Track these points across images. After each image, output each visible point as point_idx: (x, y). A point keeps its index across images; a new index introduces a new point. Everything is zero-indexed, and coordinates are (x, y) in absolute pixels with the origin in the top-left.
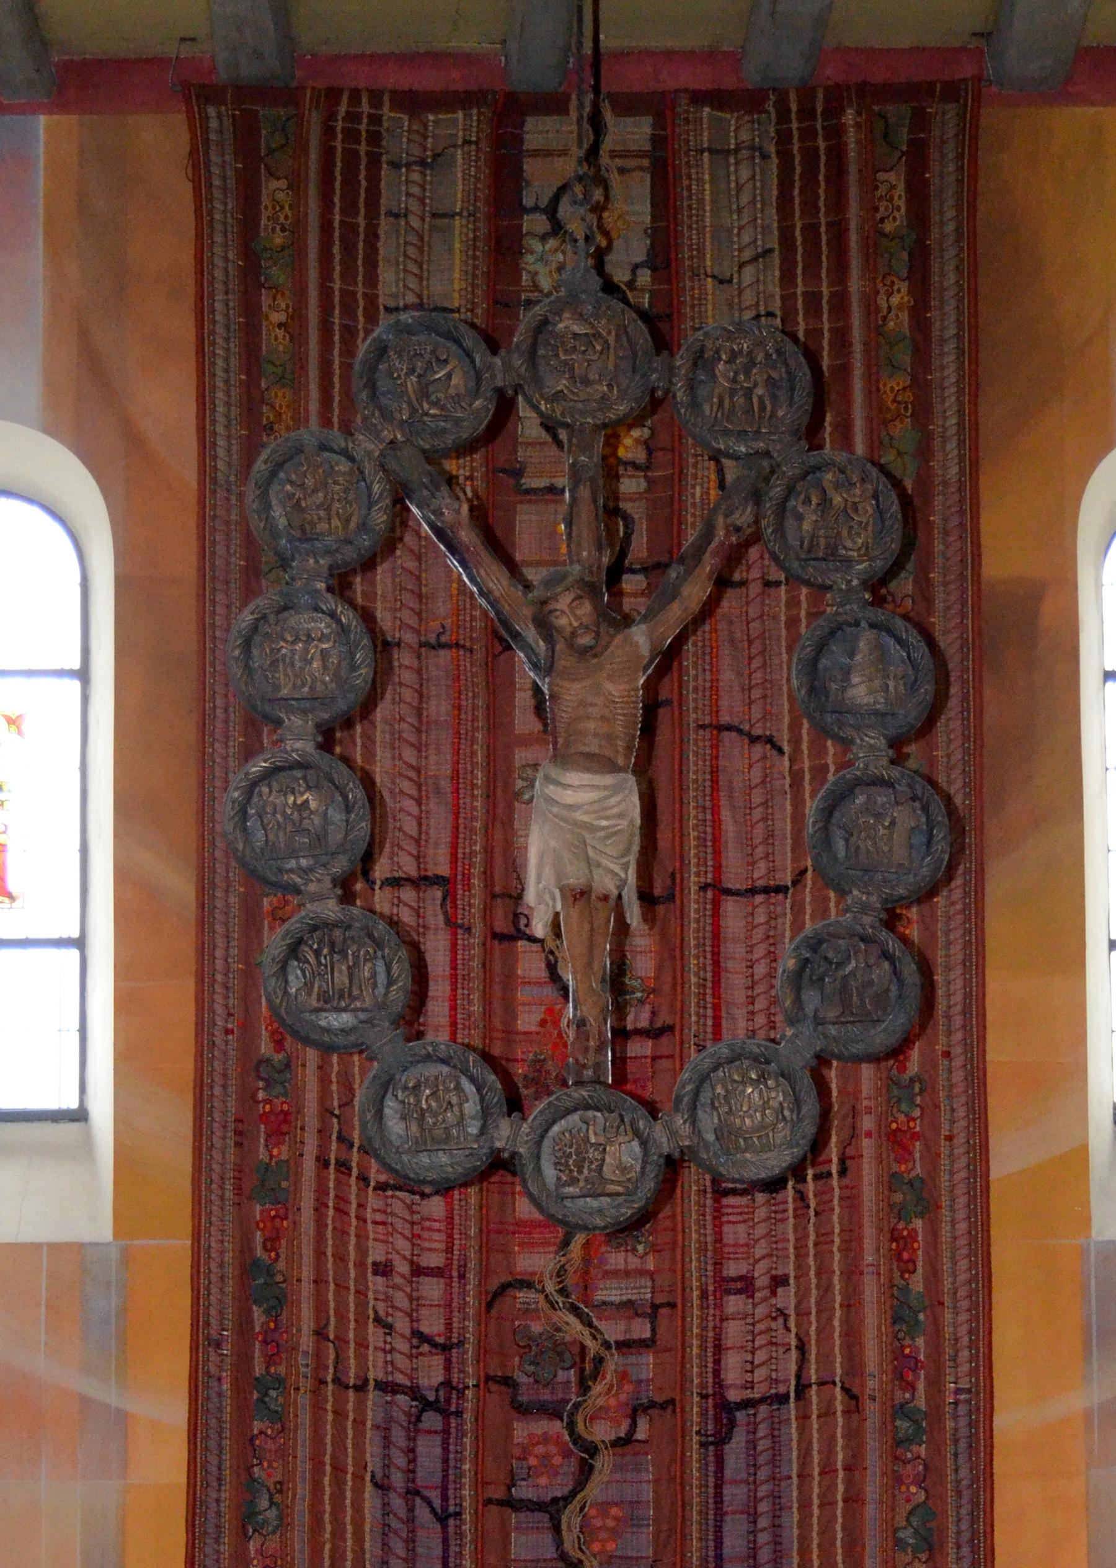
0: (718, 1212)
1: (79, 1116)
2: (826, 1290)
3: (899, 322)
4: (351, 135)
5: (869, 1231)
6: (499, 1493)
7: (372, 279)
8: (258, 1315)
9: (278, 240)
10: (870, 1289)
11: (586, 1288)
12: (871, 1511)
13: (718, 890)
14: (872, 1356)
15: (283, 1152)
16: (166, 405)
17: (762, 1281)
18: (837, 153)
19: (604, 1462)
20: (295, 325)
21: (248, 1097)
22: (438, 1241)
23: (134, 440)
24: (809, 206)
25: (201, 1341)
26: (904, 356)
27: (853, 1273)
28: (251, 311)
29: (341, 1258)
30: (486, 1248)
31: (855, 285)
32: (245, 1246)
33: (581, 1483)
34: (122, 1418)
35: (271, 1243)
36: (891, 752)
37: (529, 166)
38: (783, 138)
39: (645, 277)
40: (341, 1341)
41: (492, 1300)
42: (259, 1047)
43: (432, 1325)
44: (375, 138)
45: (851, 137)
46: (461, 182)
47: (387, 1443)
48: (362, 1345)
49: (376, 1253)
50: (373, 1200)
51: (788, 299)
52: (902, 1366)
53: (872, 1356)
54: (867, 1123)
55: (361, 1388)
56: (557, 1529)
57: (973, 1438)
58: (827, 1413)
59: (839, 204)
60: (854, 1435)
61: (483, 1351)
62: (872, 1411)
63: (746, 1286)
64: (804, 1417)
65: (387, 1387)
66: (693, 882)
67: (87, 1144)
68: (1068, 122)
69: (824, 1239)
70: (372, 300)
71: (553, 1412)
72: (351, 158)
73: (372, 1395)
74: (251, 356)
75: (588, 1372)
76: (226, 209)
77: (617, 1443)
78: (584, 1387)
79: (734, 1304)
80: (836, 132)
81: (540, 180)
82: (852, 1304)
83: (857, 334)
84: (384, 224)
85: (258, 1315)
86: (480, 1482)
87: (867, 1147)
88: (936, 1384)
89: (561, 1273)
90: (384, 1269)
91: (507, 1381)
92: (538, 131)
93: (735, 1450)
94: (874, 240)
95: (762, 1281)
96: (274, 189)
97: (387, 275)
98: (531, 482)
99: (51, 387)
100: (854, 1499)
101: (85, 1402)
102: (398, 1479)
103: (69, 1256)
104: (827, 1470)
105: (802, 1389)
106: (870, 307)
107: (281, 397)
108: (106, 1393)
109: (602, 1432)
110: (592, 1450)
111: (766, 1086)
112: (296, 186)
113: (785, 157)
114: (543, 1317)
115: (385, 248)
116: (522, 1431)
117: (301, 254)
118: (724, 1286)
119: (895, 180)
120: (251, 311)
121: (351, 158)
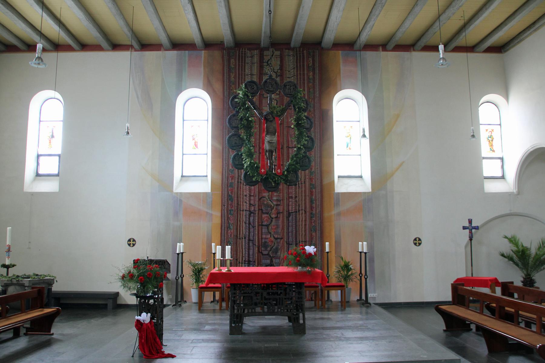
0: (288, 188)
1: (207, 176)
2: (302, 198)
3: (311, 77)
4: (242, 54)
5: (307, 191)
6: (260, 224)
7: (245, 71)
8: (230, 202)
9: (233, 66)
10: (307, 198)
11: (272, 197)
12: (307, 226)
13: (288, 147)
14: (308, 206)
15: (233, 181)
16: (218, 86)
17: (294, 197)
18: (303, 56)
19: (274, 220)
20: (235, 77)
21: (228, 174)
22: (253, 192)
23: (214, 91)
24: (300, 63)
25: (223, 205)
26: (312, 81)
27: (305, 196)
28: (229, 76)
29: (240, 194)
30: (259, 193)
31: (306, 72)
32: (228, 193)
33: (271, 223)
34: (212, 214)
35: (232, 193)
36: (283, 186)
37: (265, 57)
38: (297, 54)
39: (279, 71)
40: (240, 205)
41: (259, 199)
42: (253, 314)
43: (252, 202)
44: (245, 54)
45: (305, 54)
46: (256, 59)
47: (246, 218)
48: (243, 205)
49: (245, 194)
50: (244, 187)
51: (297, 74)
52: (312, 208)
53: (308, 206)
54: (307, 177)
55: (243, 211)
56: (268, 228)
57: (320, 217)
58: (302, 214)
59: (303, 62)
60: (306, 217)
61: (259, 206)
62: (308, 213)
63: (292, 197)
64: (299, 214)
65: (246, 211)
66: (285, 146)
67: (207, 180)
68: (332, 53)
69: (302, 192)
70: (245, 74)
71: (267, 213)
72: (242, 57)
73: (244, 212)
74: (229, 81)
75: (272, 208)
76: (226, 63)
77: (276, 217)
78: (271, 210)
79: (290, 200)
80: (303, 53)
81: (266, 59)
82: (305, 200)
83: (306, 78)
84: (246, 65)
85: (230, 202)
86: (258, 222)
87: (307, 180)
88: (316, 210)
89: (268, 196)
90: (246, 196)
91: (262, 210)
92: (266, 53)
93: (290, 218)
94: (308, 67)
95: (294, 197)
96: (232, 61)
97: (247, 71)
98: (265, 96)
99: (204, 85)
100: (305, 225)
101: (207, 212)
102: (247, 222)
103: (206, 194)
104: (302, 221)
105: (299, 211)
106: (307, 75)
107: (233, 86)
108: (210, 212)
109: (273, 216)
110: (272, 218)
111: (221, 306)
112: (235, 60)
113: (297, 56)
114: (267, 201)
115: (246, 67)
116: (264, 216)
117: (236, 67)
118: (289, 198)
119: (311, 59)
120: (229, 76)
121: (242, 57)
